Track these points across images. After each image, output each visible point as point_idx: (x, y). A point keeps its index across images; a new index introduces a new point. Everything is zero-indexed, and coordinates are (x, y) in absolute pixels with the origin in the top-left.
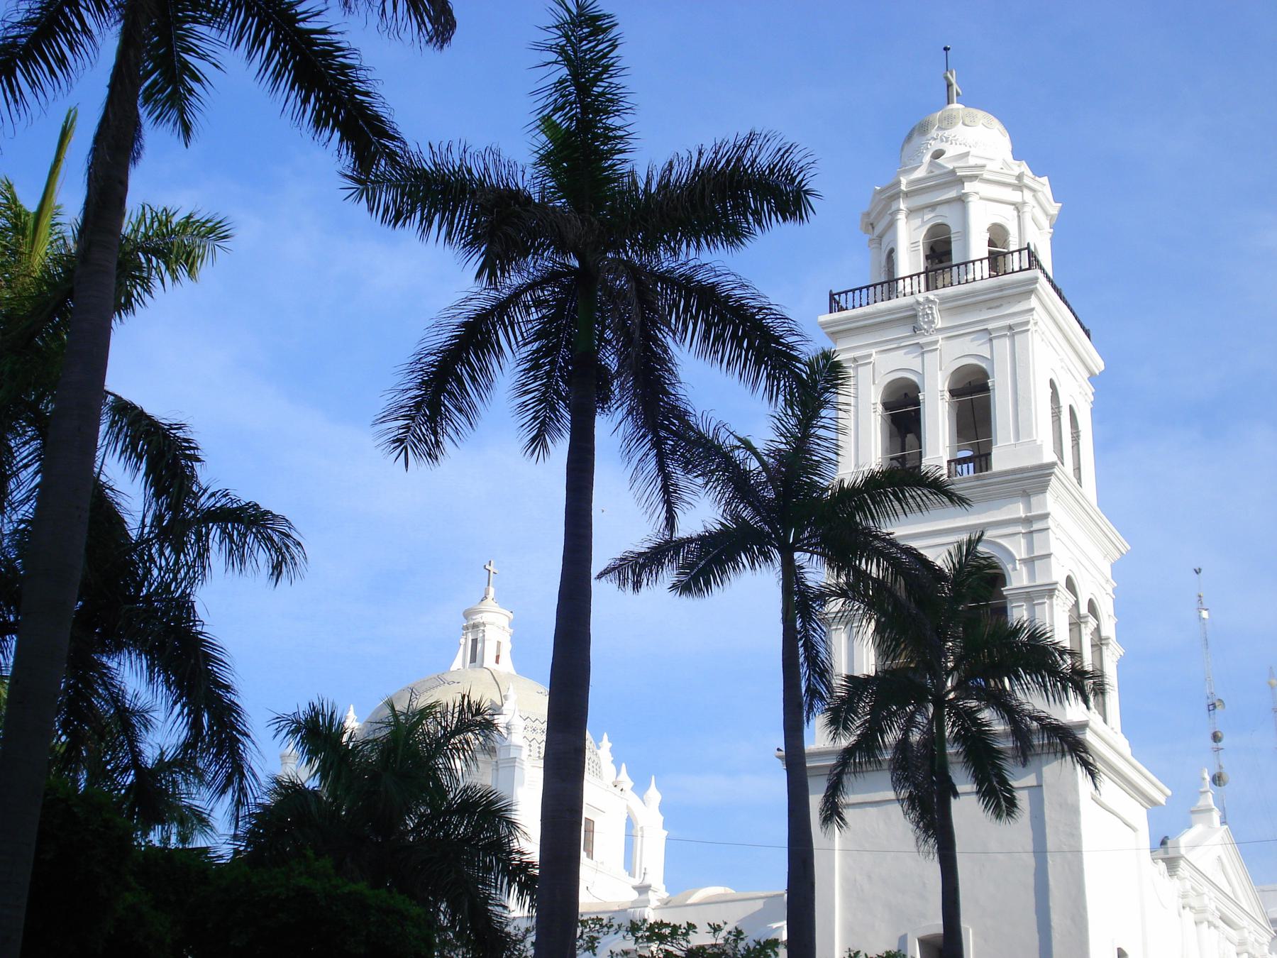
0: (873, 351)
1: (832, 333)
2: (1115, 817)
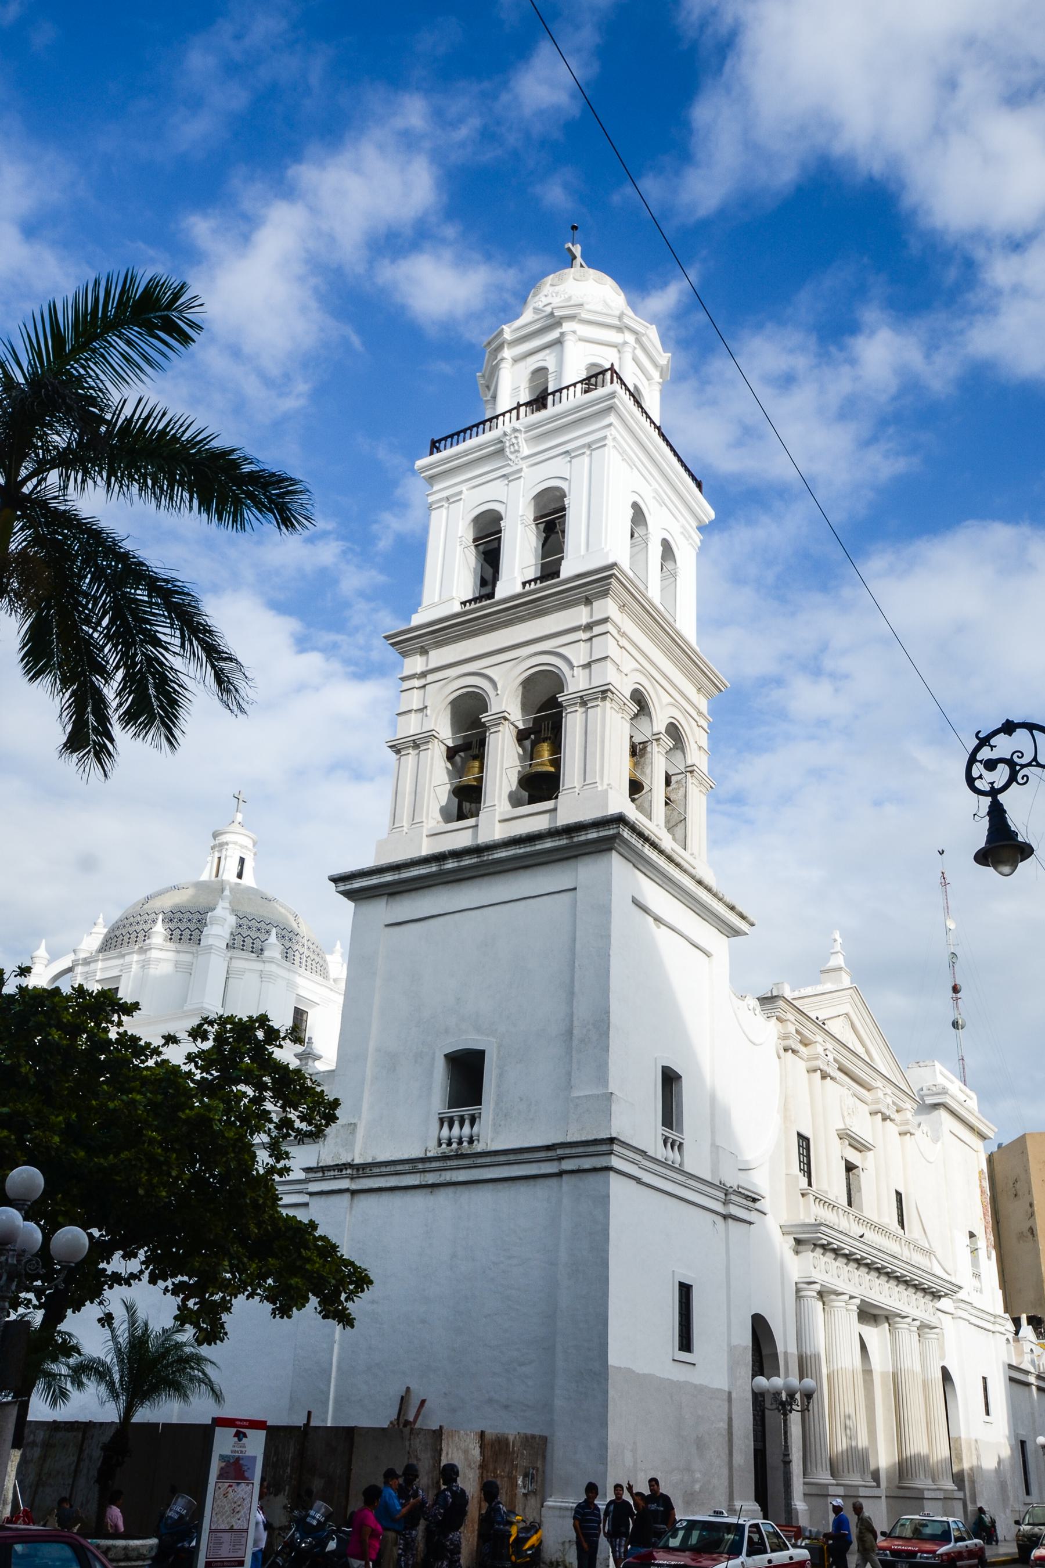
0: (464, 487)
1: (430, 478)
2: (676, 934)
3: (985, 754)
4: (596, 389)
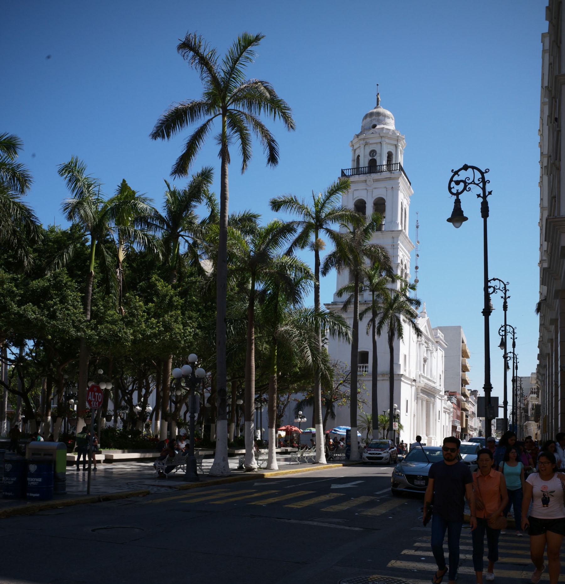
3: (456, 178)
4: (400, 163)
